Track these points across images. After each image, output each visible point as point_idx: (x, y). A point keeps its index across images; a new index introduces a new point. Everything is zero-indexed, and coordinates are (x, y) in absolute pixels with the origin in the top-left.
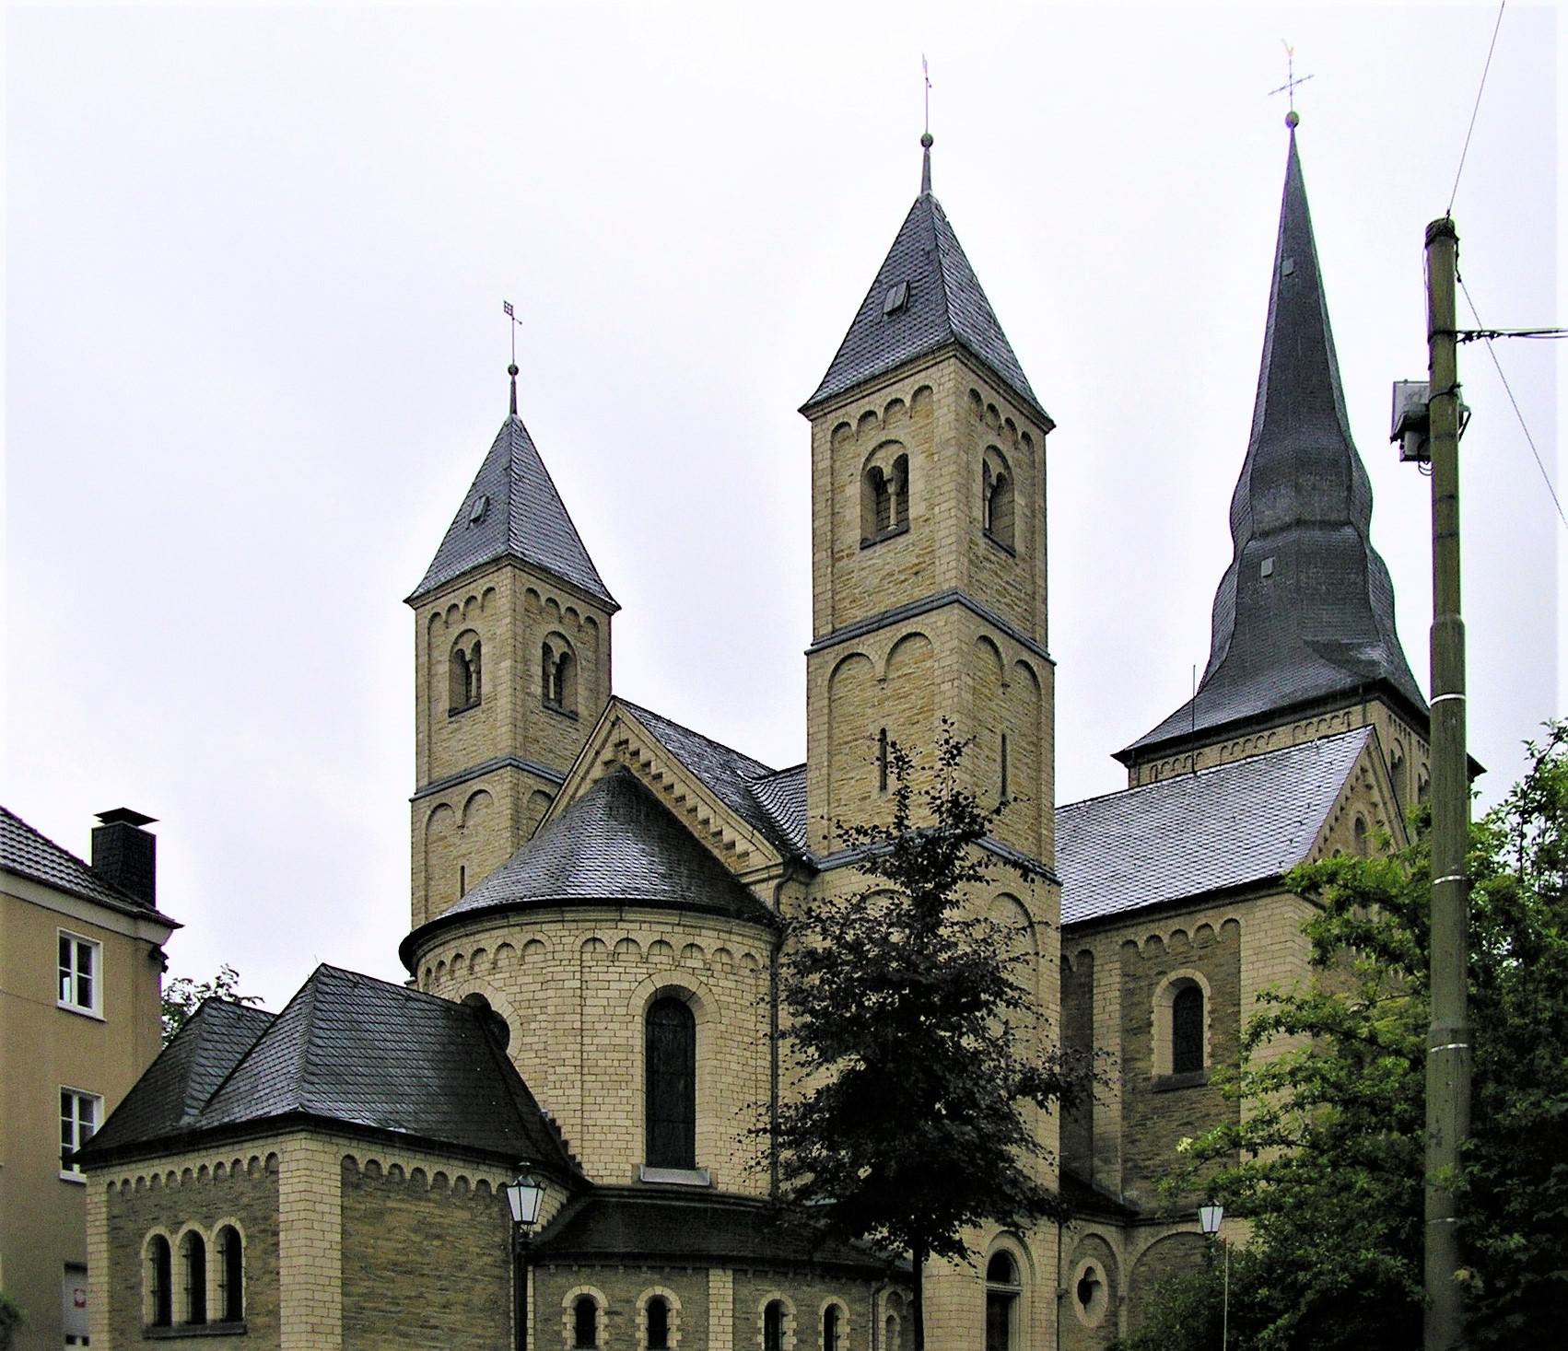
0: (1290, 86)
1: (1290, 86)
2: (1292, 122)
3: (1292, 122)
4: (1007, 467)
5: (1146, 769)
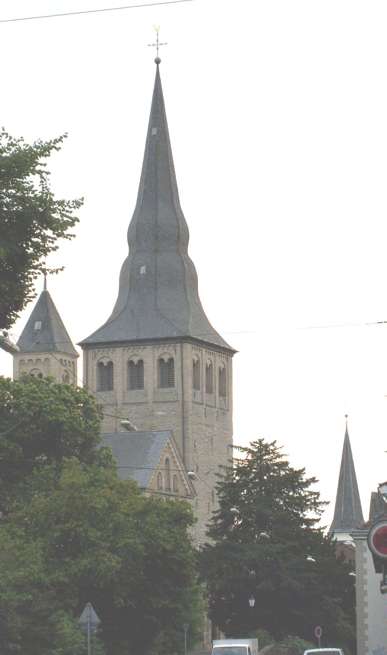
0: (158, 45)
1: (158, 45)
2: (158, 62)
3: (158, 62)
4: (68, 373)
5: (90, 352)
